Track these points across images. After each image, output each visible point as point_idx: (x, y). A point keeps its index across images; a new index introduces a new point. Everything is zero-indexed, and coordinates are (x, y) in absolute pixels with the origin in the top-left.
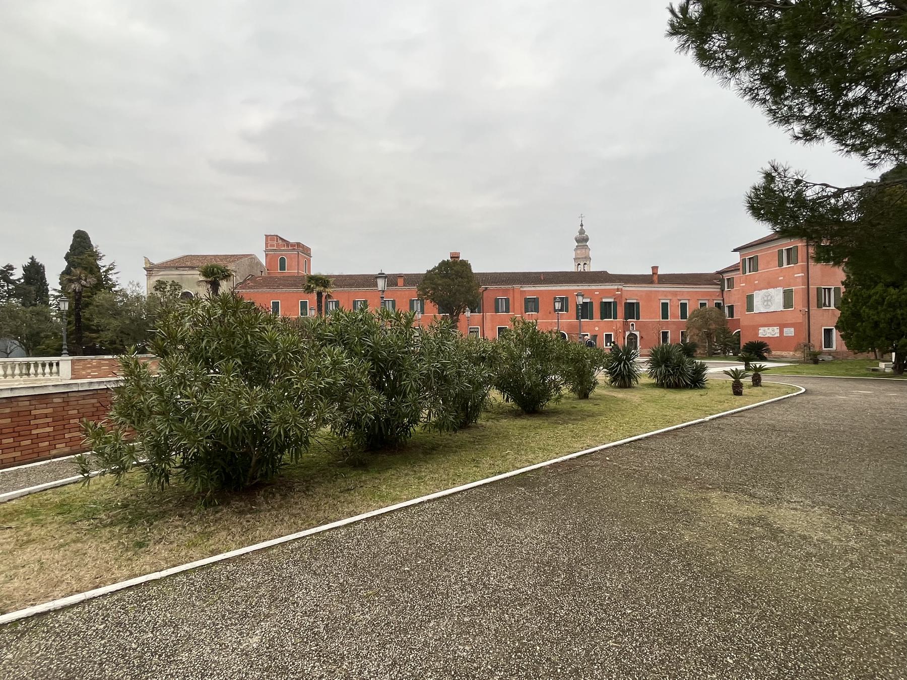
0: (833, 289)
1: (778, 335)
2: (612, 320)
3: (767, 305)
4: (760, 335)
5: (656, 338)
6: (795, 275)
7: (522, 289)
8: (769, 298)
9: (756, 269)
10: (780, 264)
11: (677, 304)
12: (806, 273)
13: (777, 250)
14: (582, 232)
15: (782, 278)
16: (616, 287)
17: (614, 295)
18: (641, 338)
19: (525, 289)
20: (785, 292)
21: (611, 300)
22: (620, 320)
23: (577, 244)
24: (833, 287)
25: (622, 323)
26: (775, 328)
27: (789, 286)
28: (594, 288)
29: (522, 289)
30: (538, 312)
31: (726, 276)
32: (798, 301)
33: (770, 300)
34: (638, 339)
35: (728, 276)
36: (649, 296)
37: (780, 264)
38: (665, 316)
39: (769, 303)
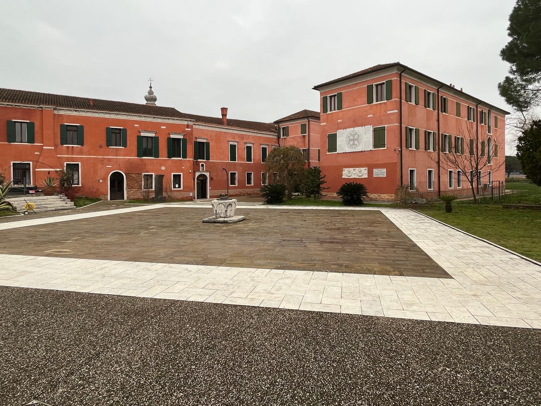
0: (414, 130)
1: (366, 176)
2: (181, 159)
3: (354, 144)
4: (343, 177)
5: (225, 178)
6: (389, 112)
7: (56, 112)
8: (356, 137)
9: (340, 107)
10: (370, 101)
11: (244, 147)
12: (399, 110)
13: (366, 86)
14: (151, 92)
15: (371, 116)
16: (186, 123)
17: (184, 132)
18: (211, 179)
19: (62, 112)
20: (375, 130)
21: (181, 137)
22: (190, 159)
23: (146, 102)
24: (414, 128)
25: (192, 162)
26: (363, 169)
27: (381, 124)
28: (159, 121)
29: (56, 112)
30: (82, 145)
31: (282, 125)
32: (391, 140)
33: (350, 140)
34: (208, 180)
35: (284, 125)
36: (218, 137)
37: (370, 101)
38: (233, 158)
39: (356, 142)
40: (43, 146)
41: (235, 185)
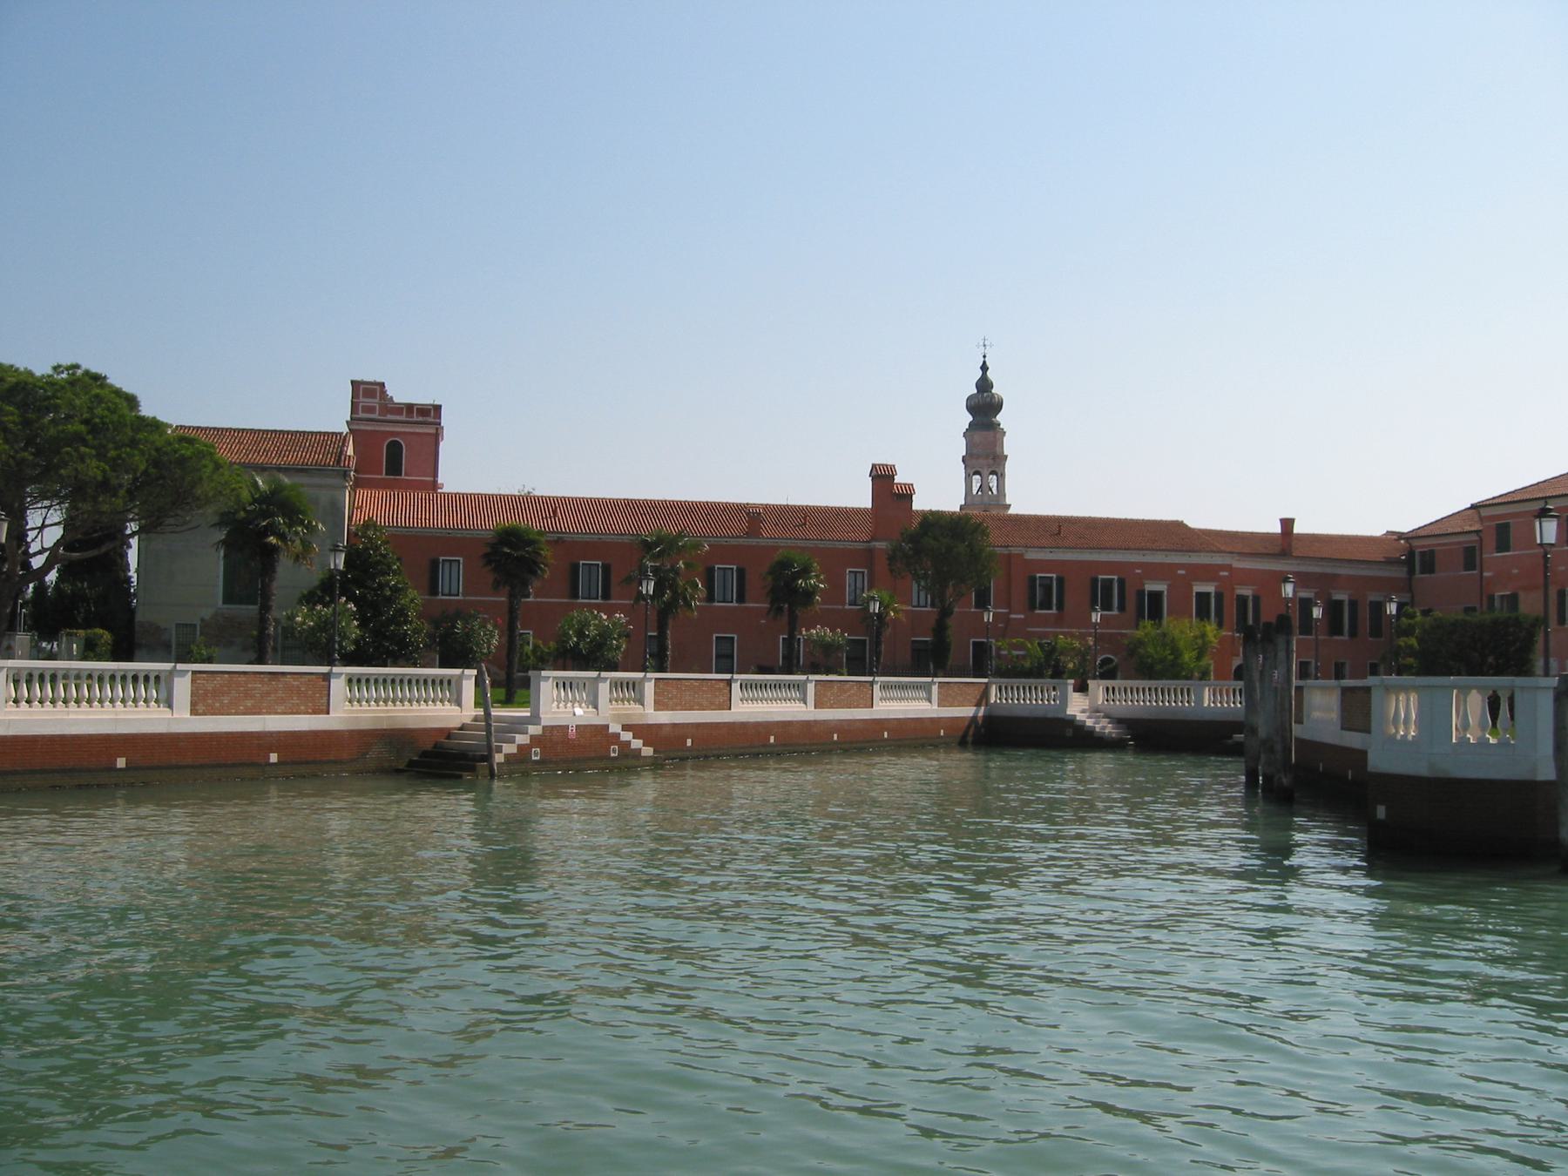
14: (984, 385)
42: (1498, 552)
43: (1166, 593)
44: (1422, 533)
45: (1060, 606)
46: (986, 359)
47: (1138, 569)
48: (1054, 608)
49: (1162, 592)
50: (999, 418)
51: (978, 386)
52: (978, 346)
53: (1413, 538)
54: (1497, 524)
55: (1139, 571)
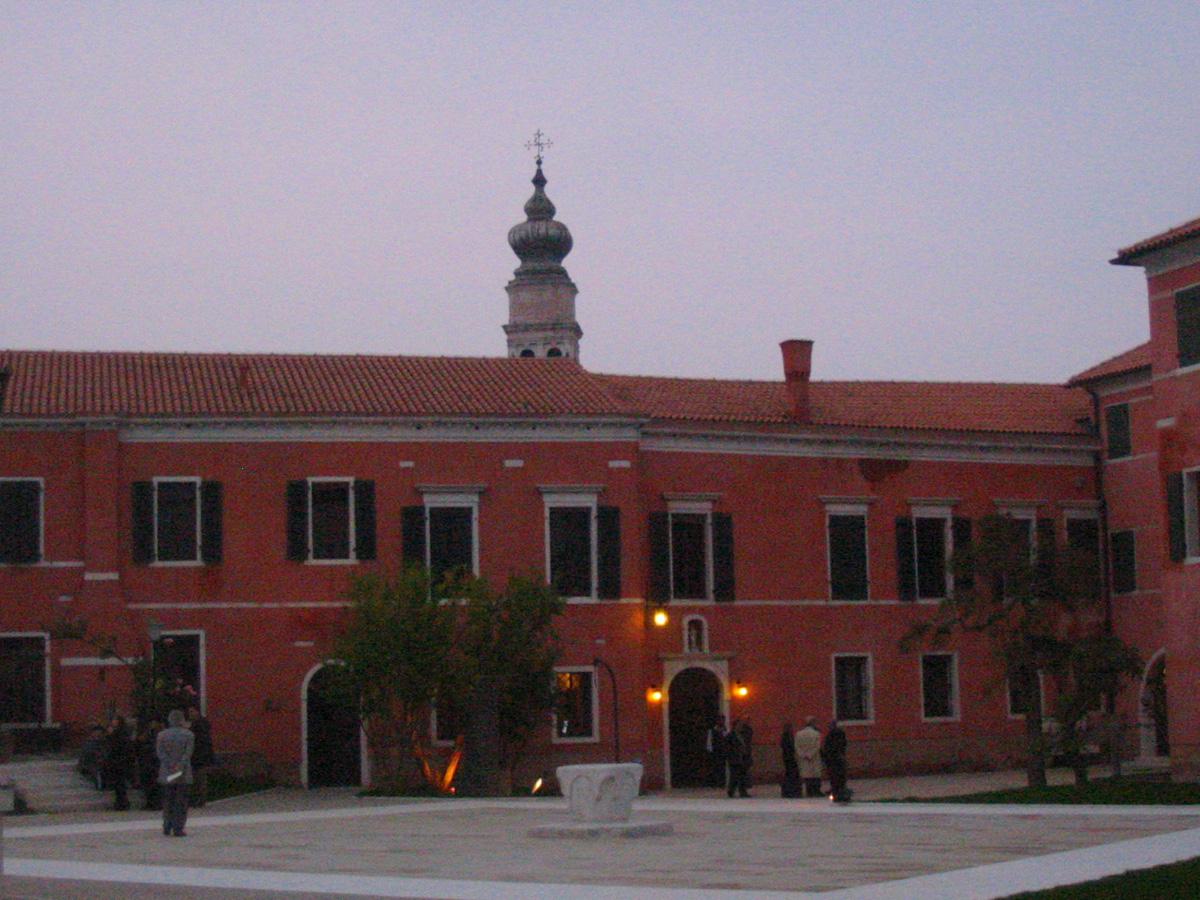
14: (540, 209)
40: (82, 571)
41: (865, 718)
42: (1183, 364)
43: (475, 514)
44: (1120, 368)
45: (213, 552)
46: (543, 167)
47: (511, 457)
48: (199, 555)
49: (466, 513)
50: (567, 263)
51: (529, 210)
52: (528, 146)
53: (1097, 379)
54: (1177, 294)
55: (404, 464)
